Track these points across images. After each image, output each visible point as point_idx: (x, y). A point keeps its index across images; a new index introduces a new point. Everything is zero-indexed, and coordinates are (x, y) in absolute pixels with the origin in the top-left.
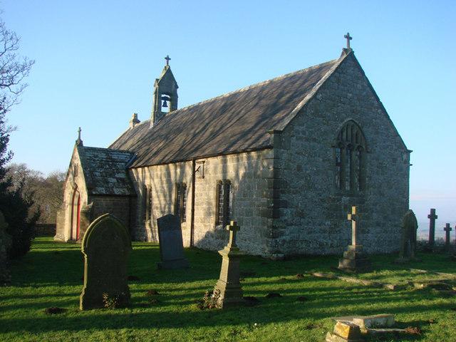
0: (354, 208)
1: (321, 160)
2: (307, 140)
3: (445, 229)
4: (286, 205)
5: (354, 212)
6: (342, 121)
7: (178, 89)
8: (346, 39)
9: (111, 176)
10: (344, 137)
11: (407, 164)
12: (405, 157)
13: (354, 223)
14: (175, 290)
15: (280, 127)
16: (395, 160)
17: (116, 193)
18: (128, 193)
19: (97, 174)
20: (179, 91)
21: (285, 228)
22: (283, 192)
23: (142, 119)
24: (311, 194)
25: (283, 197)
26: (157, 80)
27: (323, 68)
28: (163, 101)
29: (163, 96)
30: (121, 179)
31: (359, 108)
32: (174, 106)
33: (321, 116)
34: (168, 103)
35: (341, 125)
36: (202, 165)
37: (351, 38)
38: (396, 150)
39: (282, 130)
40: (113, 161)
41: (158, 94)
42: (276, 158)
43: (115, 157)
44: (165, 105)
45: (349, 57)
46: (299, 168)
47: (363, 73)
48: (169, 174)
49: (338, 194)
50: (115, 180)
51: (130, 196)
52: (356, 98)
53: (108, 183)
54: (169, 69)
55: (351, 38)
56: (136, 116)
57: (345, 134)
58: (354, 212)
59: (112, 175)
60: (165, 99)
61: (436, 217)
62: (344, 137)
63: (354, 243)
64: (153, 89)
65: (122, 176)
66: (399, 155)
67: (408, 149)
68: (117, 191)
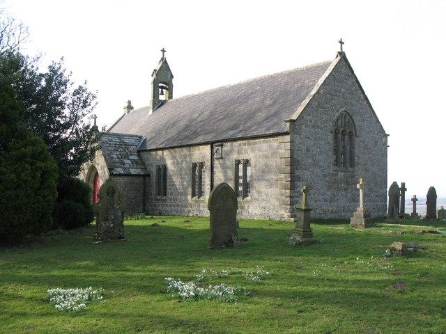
0: (361, 180)
1: (323, 143)
2: (313, 127)
3: (412, 200)
4: (298, 178)
5: (361, 183)
6: (338, 111)
7: (173, 80)
8: (340, 44)
9: (125, 157)
10: (339, 124)
11: (385, 145)
12: (384, 140)
13: (361, 191)
14: (135, 271)
15: (294, 117)
16: (376, 143)
17: (132, 173)
18: (142, 173)
19: (114, 156)
20: (174, 81)
21: (298, 197)
22: (297, 169)
23: (136, 106)
24: (317, 170)
25: (297, 173)
26: (155, 70)
27: (323, 67)
28: (160, 90)
29: (160, 85)
30: (135, 161)
31: (350, 101)
32: (170, 97)
33: (323, 108)
34: (164, 91)
35: (337, 115)
36: (220, 148)
37: (343, 43)
38: (377, 134)
39: (295, 119)
40: (126, 144)
41: (155, 83)
42: (292, 142)
43: (126, 141)
44: (162, 94)
45: (342, 55)
46: (308, 150)
47: (352, 72)
48: (218, 159)
49: (336, 171)
50: (129, 162)
51: (144, 176)
52: (347, 92)
53: (124, 164)
54: (165, 63)
55: (343, 43)
56: (130, 102)
57: (339, 122)
58: (361, 183)
59: (126, 157)
60: (162, 88)
61: (406, 190)
62: (339, 124)
63: (361, 206)
64: (152, 79)
65: (135, 157)
66: (380, 137)
67: (387, 133)
68: (133, 171)
